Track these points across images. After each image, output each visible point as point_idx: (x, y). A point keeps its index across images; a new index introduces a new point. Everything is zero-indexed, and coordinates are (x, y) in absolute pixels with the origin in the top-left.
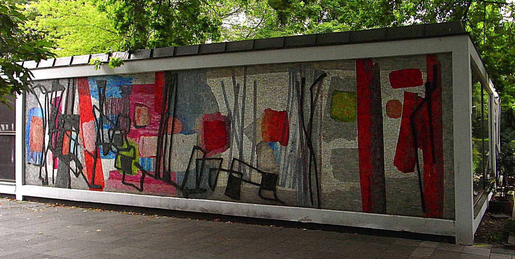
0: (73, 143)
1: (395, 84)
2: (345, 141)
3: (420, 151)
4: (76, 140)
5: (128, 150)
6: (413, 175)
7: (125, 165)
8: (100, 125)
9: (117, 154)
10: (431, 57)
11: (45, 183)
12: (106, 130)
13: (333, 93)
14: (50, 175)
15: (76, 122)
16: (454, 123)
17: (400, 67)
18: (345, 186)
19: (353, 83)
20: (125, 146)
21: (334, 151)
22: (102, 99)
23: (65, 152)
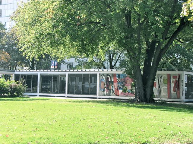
0: (112, 87)
1: (173, 78)
2: (165, 87)
3: (177, 89)
4: (113, 86)
5: (125, 88)
6: (176, 92)
7: (124, 91)
8: (118, 83)
9: (122, 89)
10: (179, 74)
11: (104, 95)
12: (120, 84)
13: (164, 79)
14: (106, 93)
15: (113, 82)
16: (15, 101)
17: (174, 75)
18: (165, 94)
19: (167, 78)
20: (124, 87)
21: (164, 89)
22: (119, 78)
23: (110, 88)
